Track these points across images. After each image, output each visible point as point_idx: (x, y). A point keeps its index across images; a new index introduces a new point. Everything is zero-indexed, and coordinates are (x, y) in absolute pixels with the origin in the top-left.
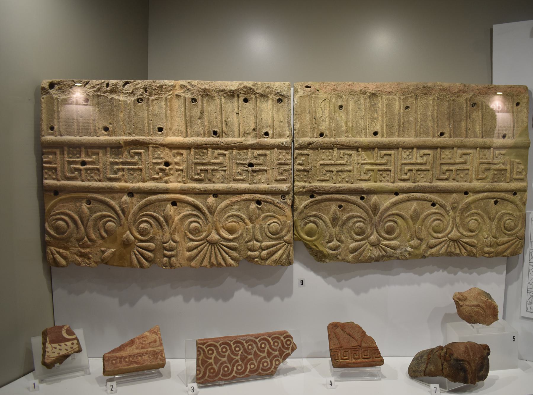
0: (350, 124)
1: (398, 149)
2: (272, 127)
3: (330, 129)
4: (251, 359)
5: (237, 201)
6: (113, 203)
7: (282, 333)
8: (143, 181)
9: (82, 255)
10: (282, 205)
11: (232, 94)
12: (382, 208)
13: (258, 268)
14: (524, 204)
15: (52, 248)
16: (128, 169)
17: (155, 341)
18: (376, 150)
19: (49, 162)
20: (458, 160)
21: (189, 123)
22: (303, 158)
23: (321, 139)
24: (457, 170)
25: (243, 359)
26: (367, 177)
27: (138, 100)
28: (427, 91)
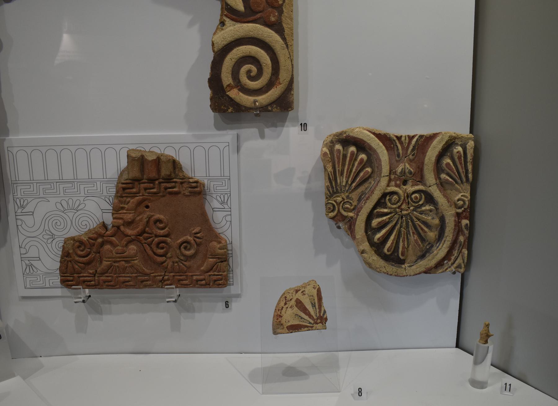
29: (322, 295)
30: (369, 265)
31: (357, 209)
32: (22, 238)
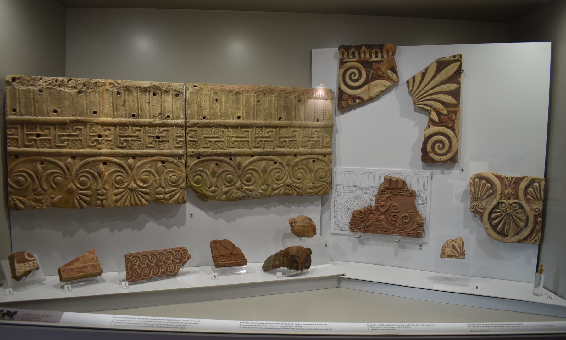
0: (223, 111)
1: (253, 127)
2: (172, 112)
3: (210, 114)
4: (162, 265)
5: (149, 161)
6: (60, 163)
7: (181, 248)
8: (83, 148)
9: (36, 201)
10: (179, 164)
11: (145, 90)
12: (244, 165)
13: (161, 206)
14: (331, 162)
15: (13, 197)
16: (72, 140)
17: (93, 258)
18: (239, 128)
19: (12, 135)
20: (290, 135)
21: (115, 109)
22: (193, 133)
23: (204, 121)
24: (290, 141)
25: (156, 265)
26: (234, 146)
27: (79, 92)
28: (271, 91)
29: (358, 109)
30: (490, 235)
31: (484, 209)
32: (336, 208)
